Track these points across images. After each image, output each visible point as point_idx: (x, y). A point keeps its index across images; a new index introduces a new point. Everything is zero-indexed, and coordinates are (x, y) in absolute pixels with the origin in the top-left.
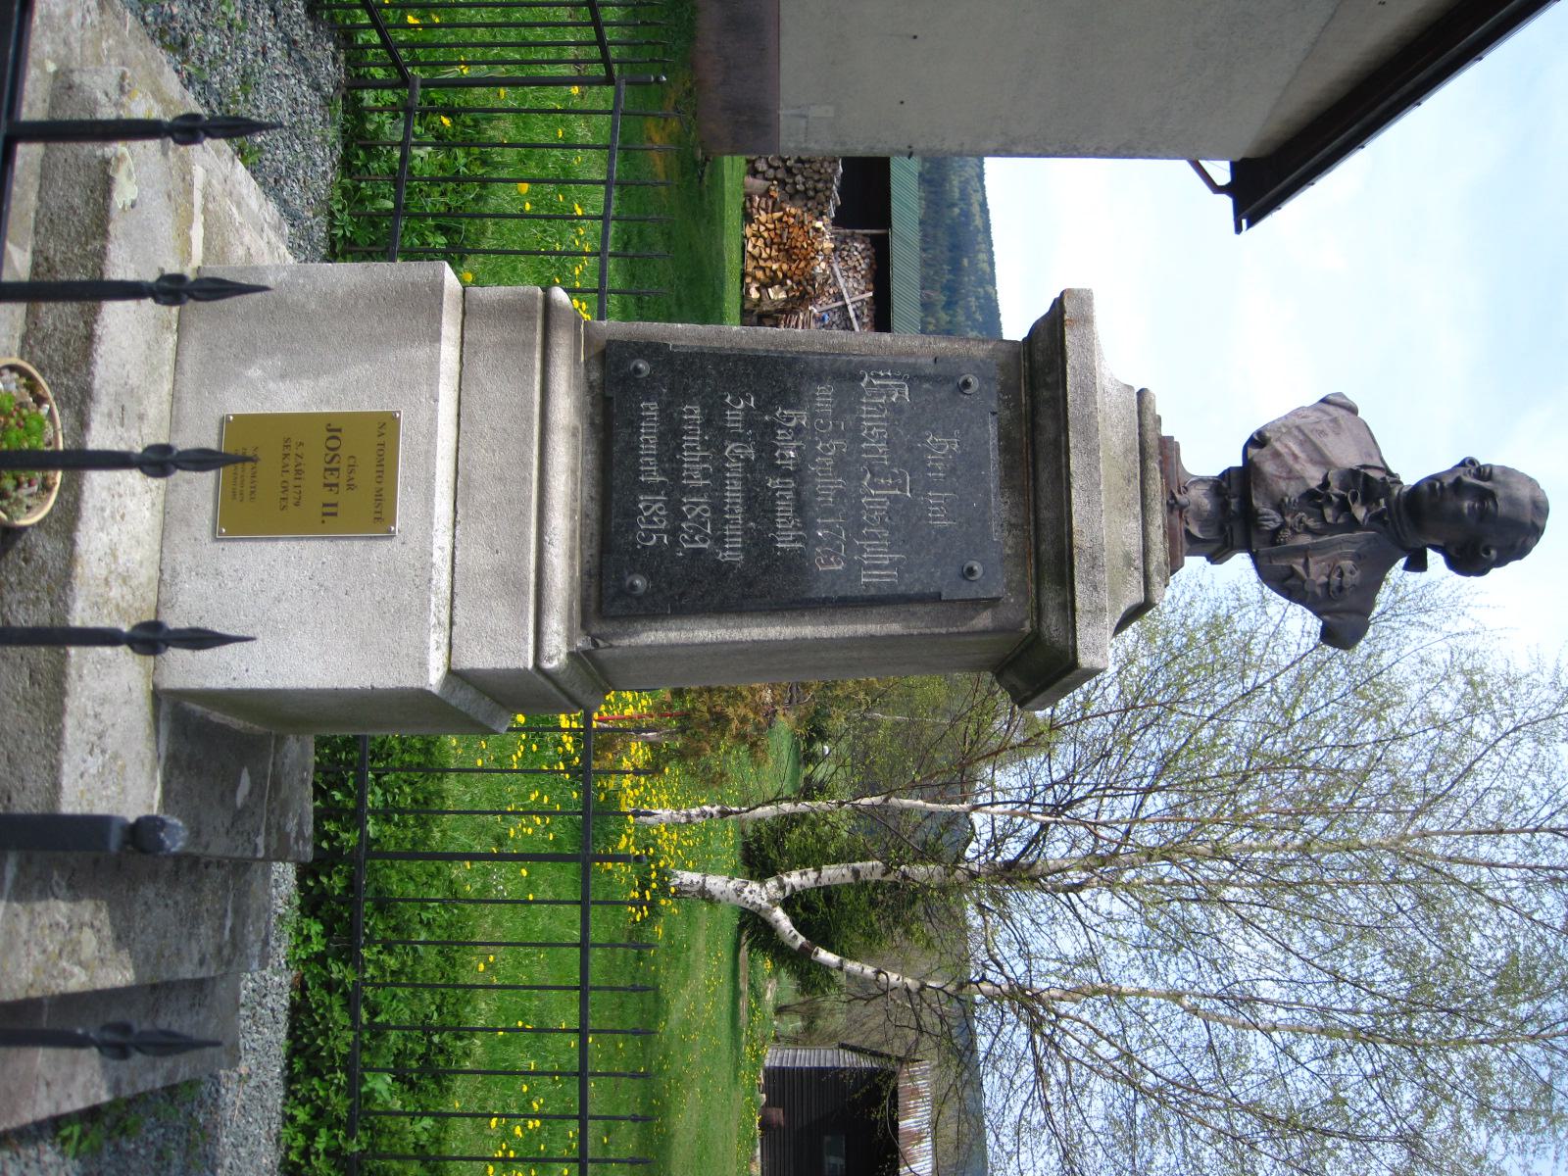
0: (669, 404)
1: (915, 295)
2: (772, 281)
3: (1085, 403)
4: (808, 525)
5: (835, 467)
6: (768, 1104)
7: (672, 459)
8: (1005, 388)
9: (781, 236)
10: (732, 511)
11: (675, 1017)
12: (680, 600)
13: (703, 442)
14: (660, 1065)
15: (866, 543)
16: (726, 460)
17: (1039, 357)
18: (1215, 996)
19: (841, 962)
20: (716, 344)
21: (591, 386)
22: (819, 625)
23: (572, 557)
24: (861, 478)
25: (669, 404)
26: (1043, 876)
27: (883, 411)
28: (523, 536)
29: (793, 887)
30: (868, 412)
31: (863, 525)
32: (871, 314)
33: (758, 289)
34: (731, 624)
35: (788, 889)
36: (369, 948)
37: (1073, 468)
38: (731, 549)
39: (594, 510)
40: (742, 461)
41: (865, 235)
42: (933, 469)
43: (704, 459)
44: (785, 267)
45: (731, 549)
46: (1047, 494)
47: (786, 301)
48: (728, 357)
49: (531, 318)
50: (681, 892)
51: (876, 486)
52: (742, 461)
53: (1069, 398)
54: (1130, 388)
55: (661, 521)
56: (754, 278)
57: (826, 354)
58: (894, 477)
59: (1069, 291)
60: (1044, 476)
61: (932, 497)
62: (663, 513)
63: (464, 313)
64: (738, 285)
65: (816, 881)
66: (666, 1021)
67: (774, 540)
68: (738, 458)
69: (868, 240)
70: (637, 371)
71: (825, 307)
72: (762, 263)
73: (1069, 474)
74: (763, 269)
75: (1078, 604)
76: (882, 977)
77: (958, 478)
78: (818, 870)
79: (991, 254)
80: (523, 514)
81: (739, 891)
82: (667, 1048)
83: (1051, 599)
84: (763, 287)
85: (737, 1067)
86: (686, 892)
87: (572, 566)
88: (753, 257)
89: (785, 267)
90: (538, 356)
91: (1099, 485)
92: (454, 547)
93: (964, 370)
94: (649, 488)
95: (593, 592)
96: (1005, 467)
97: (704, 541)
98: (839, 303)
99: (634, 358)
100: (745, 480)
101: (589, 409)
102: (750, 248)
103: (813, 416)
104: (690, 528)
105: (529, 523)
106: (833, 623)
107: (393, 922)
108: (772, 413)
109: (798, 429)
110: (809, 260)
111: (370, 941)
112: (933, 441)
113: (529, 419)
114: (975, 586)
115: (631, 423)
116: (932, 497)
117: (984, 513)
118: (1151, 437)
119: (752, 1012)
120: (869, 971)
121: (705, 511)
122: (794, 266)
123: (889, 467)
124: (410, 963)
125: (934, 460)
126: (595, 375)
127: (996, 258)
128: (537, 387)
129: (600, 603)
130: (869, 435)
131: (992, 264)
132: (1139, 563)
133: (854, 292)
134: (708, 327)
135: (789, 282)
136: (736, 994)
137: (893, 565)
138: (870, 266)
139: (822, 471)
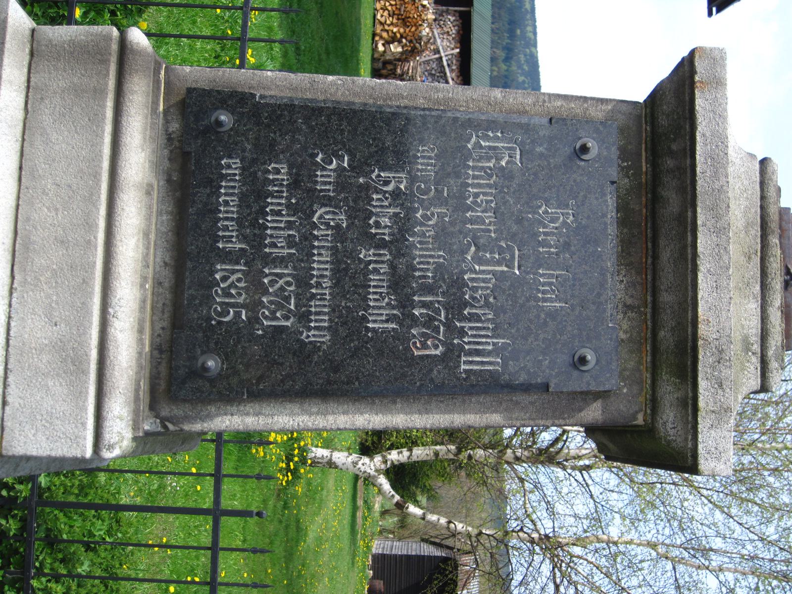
0: (254, 161)
1: (487, 52)
2: (393, 39)
3: (716, 175)
4: (405, 304)
5: (436, 238)
6: (374, 577)
7: (254, 224)
8: (624, 154)
9: (400, 9)
10: (319, 285)
11: (311, 535)
12: (258, 383)
13: (289, 206)
14: (300, 571)
15: (467, 325)
16: (314, 226)
17: (663, 121)
18: (680, 546)
19: (424, 514)
20: (309, 96)
21: (170, 139)
22: (411, 413)
23: (141, 331)
24: (464, 252)
25: (254, 161)
26: (567, 460)
27: (491, 176)
28: (85, 308)
29: (392, 461)
30: (475, 177)
31: (466, 304)
32: (458, 63)
33: (383, 45)
34: (315, 410)
35: (389, 463)
36: (38, 579)
37: (700, 249)
38: (316, 328)
39: (167, 276)
40: (332, 228)
41: (455, 11)
42: (545, 244)
43: (290, 225)
44: (402, 30)
45: (316, 328)
46: (668, 275)
47: (402, 53)
48: (321, 110)
49: (105, 62)
50: (315, 463)
51: (481, 261)
52: (332, 228)
53: (698, 170)
54: (753, 156)
55: (240, 294)
56: (381, 37)
57: (430, 109)
58: (501, 251)
59: (701, 48)
60: (666, 255)
61: (542, 275)
62: (242, 285)
63: (32, 54)
64: (370, 41)
65: (409, 458)
66: (305, 542)
67: (365, 319)
68: (327, 225)
69: (457, 14)
70: (219, 124)
71: (428, 58)
72: (386, 27)
73: (695, 255)
74: (387, 31)
75: (701, 404)
76: (452, 526)
77: (572, 254)
78: (410, 450)
79: (535, 27)
80: (86, 282)
81: (355, 464)
82: (305, 559)
83: (669, 392)
84: (387, 43)
85: (354, 556)
86: (318, 463)
87: (140, 341)
88: (381, 23)
89: (402, 30)
90: (110, 104)
91: (728, 268)
92: (10, 317)
93: (582, 133)
94: (228, 256)
95: (163, 369)
96: (621, 241)
97: (287, 318)
98: (437, 56)
99: (216, 109)
100: (334, 250)
101: (167, 164)
102: (379, 17)
103: (412, 179)
104: (271, 302)
105: (92, 293)
106: (427, 412)
107: (60, 556)
108: (367, 175)
109: (396, 194)
110: (418, 26)
111: (40, 573)
112: (546, 212)
113: (96, 176)
114: (587, 377)
115: (210, 182)
116: (542, 275)
117: (599, 295)
118: (773, 210)
119: (365, 518)
120: (443, 521)
121: (288, 284)
122: (407, 30)
123: (497, 239)
124: (74, 588)
125: (545, 234)
126: (175, 126)
127: (538, 30)
128: (107, 139)
129: (170, 384)
130: (475, 203)
131: (535, 33)
132: (756, 347)
133: (447, 49)
134: (300, 76)
135: (404, 41)
136: (355, 508)
137: (497, 351)
138: (458, 32)
139: (420, 242)
